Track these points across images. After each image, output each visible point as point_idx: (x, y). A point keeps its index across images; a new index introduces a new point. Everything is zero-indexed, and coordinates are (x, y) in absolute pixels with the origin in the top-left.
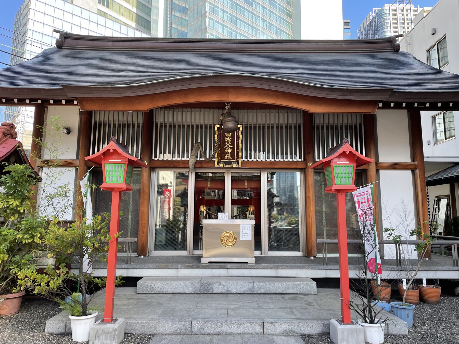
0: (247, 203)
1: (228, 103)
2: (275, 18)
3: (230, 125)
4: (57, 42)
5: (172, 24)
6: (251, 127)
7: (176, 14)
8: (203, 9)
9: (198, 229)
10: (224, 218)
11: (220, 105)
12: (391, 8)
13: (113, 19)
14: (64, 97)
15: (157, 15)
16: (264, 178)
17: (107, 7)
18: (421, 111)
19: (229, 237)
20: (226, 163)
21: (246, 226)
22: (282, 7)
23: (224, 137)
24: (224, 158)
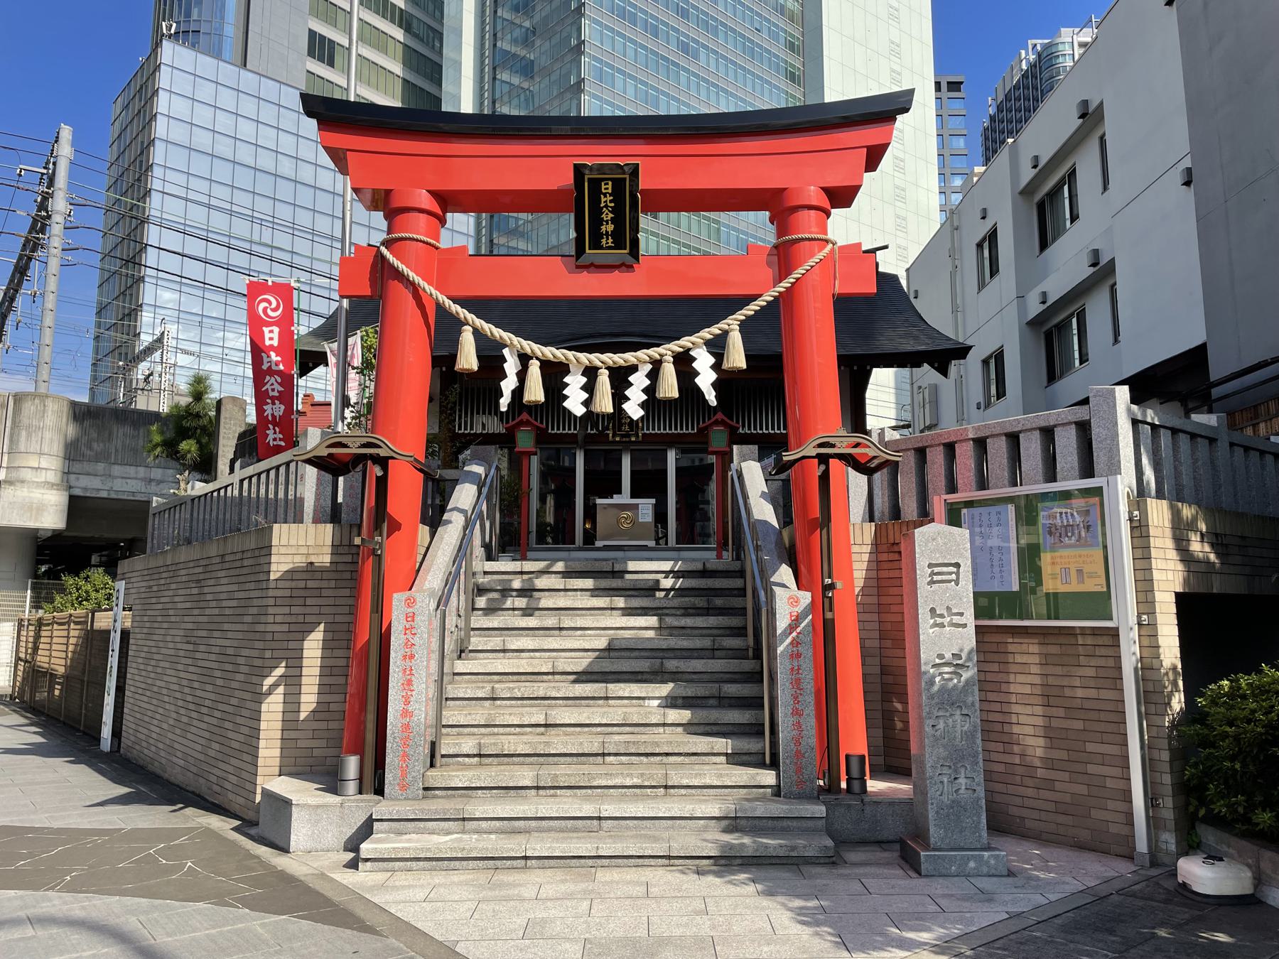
2: (758, 88)
5: (495, 40)
7: (507, 15)
8: (574, 71)
9: (590, 512)
10: (624, 498)
12: (1077, 39)
15: (458, 47)
17: (331, 64)
18: (875, 370)
20: (622, 436)
21: (646, 507)
22: (777, 57)
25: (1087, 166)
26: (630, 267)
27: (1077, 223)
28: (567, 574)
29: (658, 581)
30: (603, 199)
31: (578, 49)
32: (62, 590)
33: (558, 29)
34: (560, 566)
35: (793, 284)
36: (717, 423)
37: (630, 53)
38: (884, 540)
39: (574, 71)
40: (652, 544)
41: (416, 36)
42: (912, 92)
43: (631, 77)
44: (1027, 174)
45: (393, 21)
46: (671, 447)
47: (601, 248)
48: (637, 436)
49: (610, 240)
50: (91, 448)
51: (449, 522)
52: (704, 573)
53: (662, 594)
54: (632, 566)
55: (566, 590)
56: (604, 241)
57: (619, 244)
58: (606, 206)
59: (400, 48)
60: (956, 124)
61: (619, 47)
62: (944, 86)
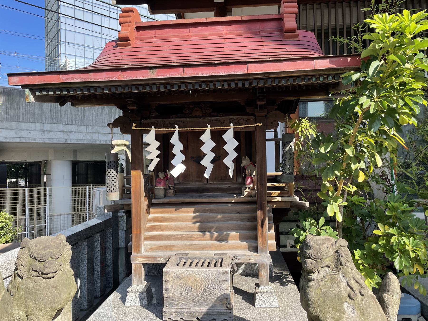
15: (168, 212)
32: (310, 272)
42: (157, 149)
50: (7, 114)
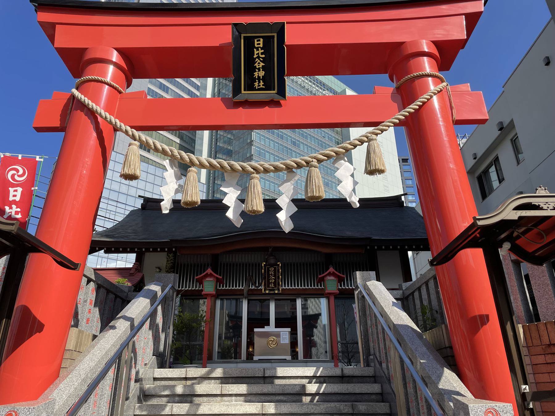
0: (286, 321)
1: (271, 247)
3: (272, 261)
4: (142, 205)
6: (291, 265)
8: (249, 152)
9: (250, 343)
10: (271, 328)
11: (265, 249)
13: (154, 164)
14: (155, 247)
16: (299, 302)
19: (273, 341)
20: (270, 290)
21: (285, 332)
23: (269, 271)
24: (269, 287)
25: (506, 154)
26: (277, 104)
27: (503, 183)
28: (225, 380)
29: (304, 387)
30: (256, 52)
31: (251, 144)
33: (242, 136)
34: (218, 372)
35: (420, 107)
36: (330, 274)
37: (272, 145)
38: (536, 342)
39: (249, 152)
40: (289, 358)
41: (185, 141)
43: (272, 154)
44: (471, 162)
45: (175, 136)
46: (298, 297)
47: (255, 89)
48: (279, 290)
49: (262, 83)
51: (113, 327)
52: (343, 378)
53: (308, 399)
54: (281, 371)
55: (222, 395)
56: (256, 84)
57: (268, 87)
58: (258, 57)
59: (178, 145)
60: (407, 175)
61: (267, 143)
62: (401, 161)
